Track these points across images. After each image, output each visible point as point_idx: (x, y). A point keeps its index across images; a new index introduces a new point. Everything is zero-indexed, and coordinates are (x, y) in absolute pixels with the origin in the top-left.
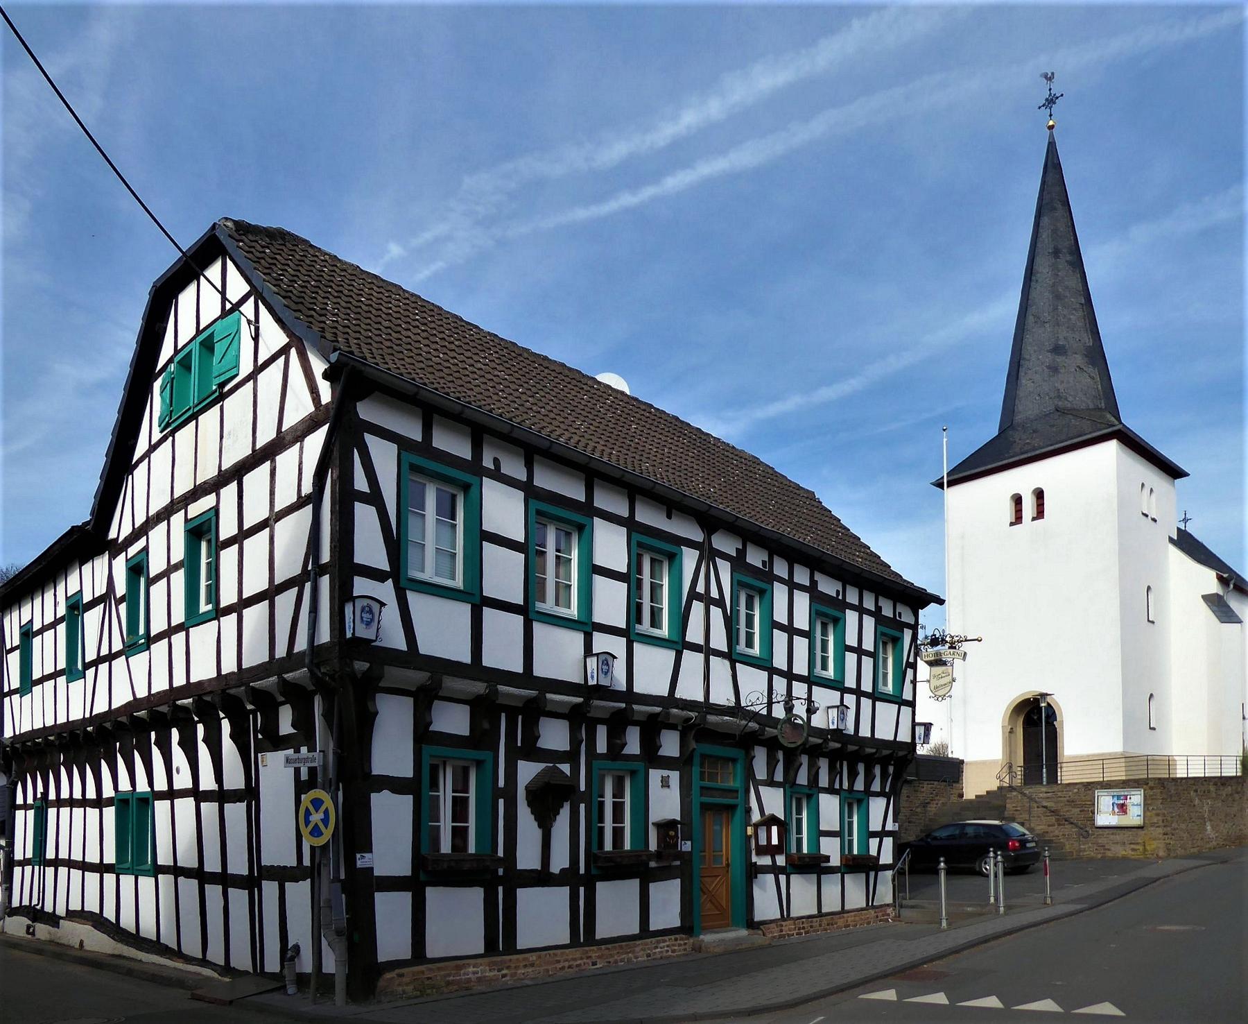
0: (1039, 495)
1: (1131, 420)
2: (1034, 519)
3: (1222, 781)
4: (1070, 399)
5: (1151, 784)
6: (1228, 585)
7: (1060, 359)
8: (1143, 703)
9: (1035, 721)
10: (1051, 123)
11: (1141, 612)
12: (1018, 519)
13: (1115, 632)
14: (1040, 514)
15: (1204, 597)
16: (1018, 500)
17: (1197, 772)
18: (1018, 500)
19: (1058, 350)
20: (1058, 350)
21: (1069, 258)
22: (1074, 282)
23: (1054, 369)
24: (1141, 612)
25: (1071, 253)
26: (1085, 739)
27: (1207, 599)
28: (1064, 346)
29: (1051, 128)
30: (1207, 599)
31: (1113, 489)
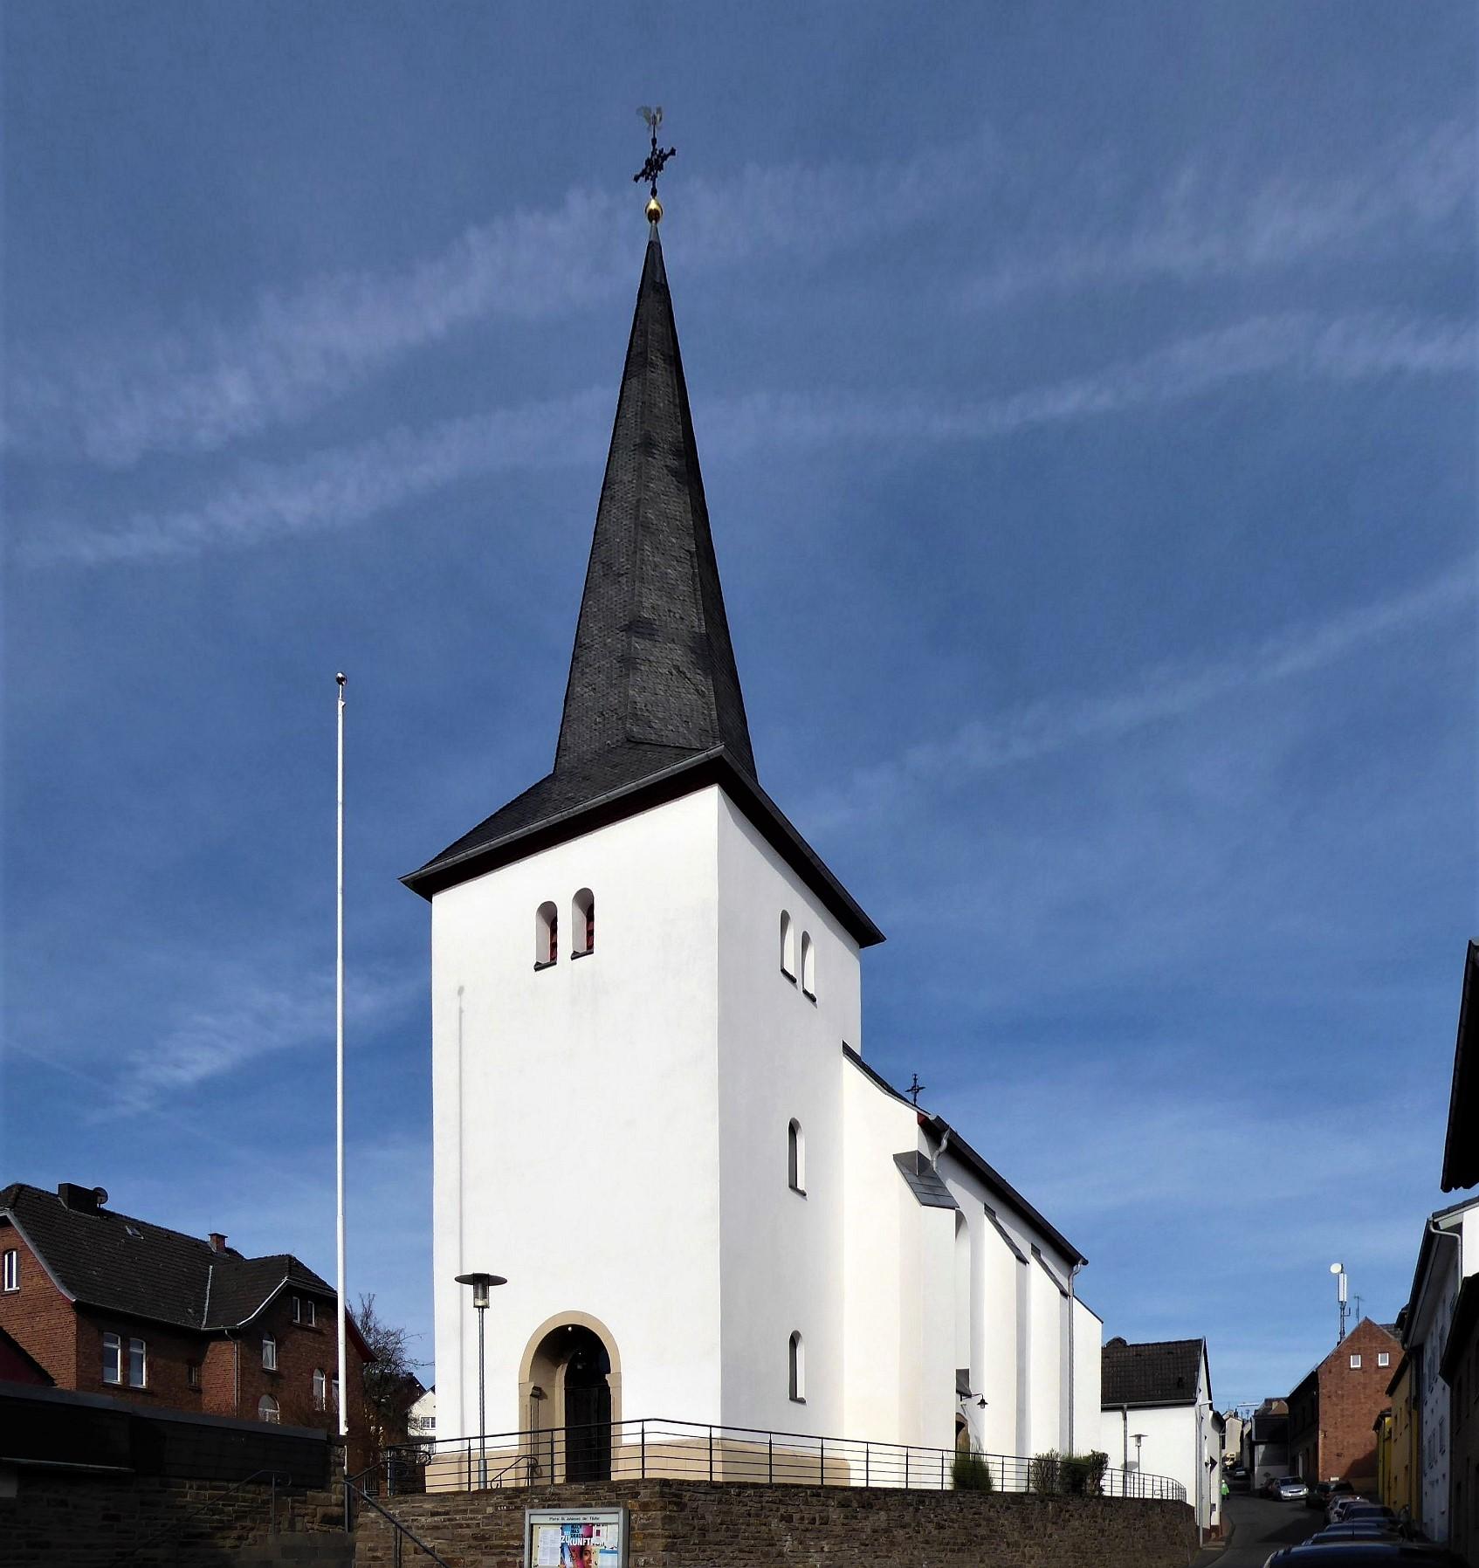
0: (585, 902)
1: (770, 778)
2: (575, 956)
3: (923, 1495)
4: (657, 725)
5: (645, 1495)
6: (939, 1144)
7: (639, 645)
8: (774, 1349)
9: (575, 1359)
10: (653, 205)
11: (774, 1165)
12: (547, 961)
13: (706, 1194)
14: (588, 947)
15: (899, 1159)
16: (548, 913)
17: (887, 1476)
18: (548, 913)
19: (637, 627)
20: (637, 627)
21: (672, 462)
22: (677, 506)
23: (628, 663)
24: (774, 1165)
25: (677, 454)
26: (668, 1404)
27: (902, 1160)
28: (649, 622)
29: (654, 216)
30: (902, 1160)
31: (711, 891)
